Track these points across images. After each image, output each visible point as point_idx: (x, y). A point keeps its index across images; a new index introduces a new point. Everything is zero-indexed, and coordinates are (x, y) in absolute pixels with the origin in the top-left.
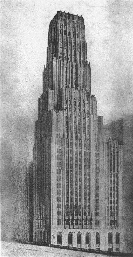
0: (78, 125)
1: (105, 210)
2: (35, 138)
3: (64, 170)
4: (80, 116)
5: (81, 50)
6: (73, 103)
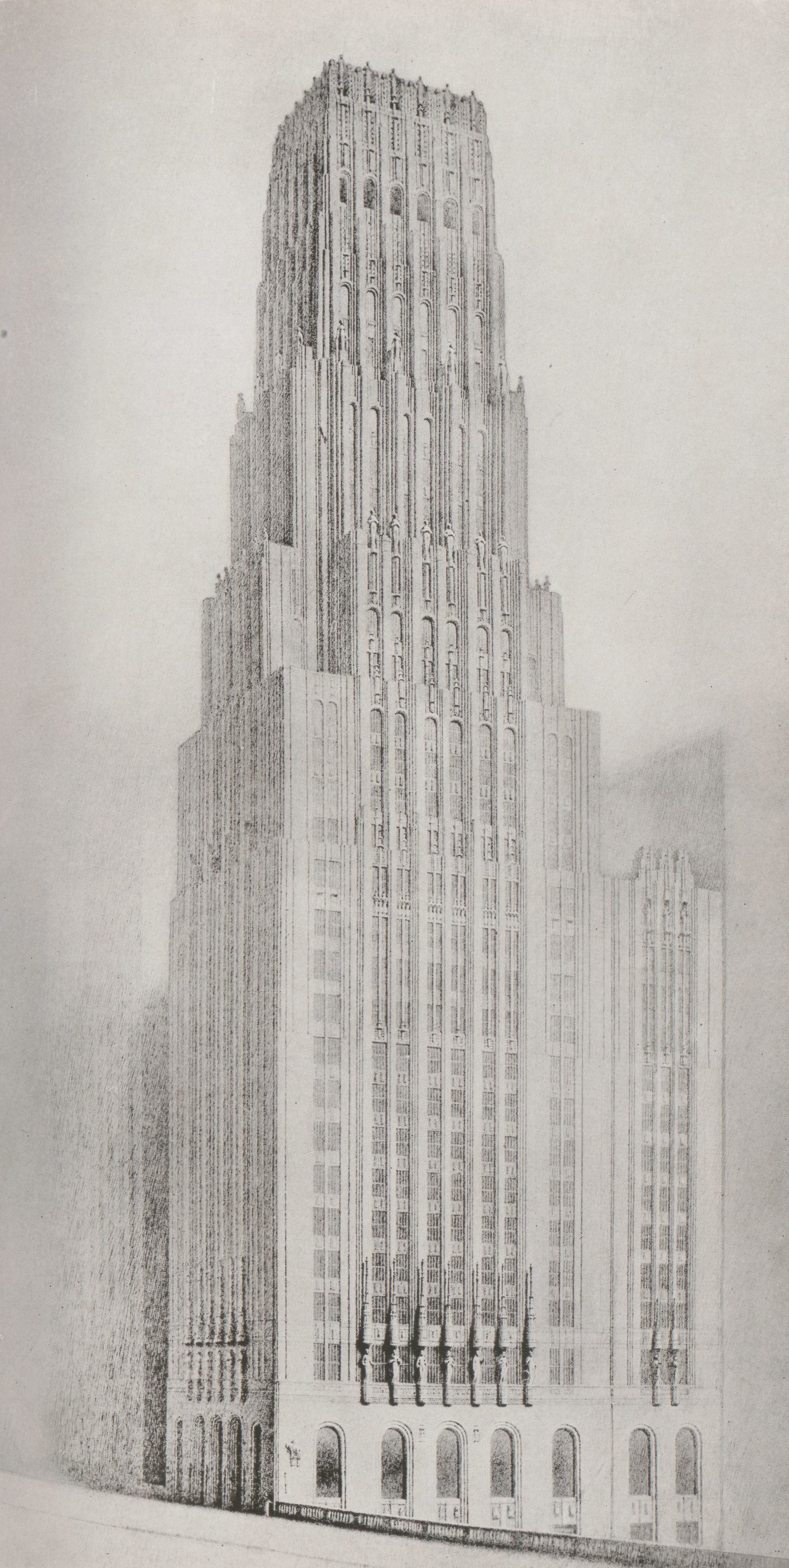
0: (446, 765)
1: (612, 1291)
2: (183, 842)
3: (359, 1040)
4: (462, 708)
5: (470, 305)
6: (419, 630)
